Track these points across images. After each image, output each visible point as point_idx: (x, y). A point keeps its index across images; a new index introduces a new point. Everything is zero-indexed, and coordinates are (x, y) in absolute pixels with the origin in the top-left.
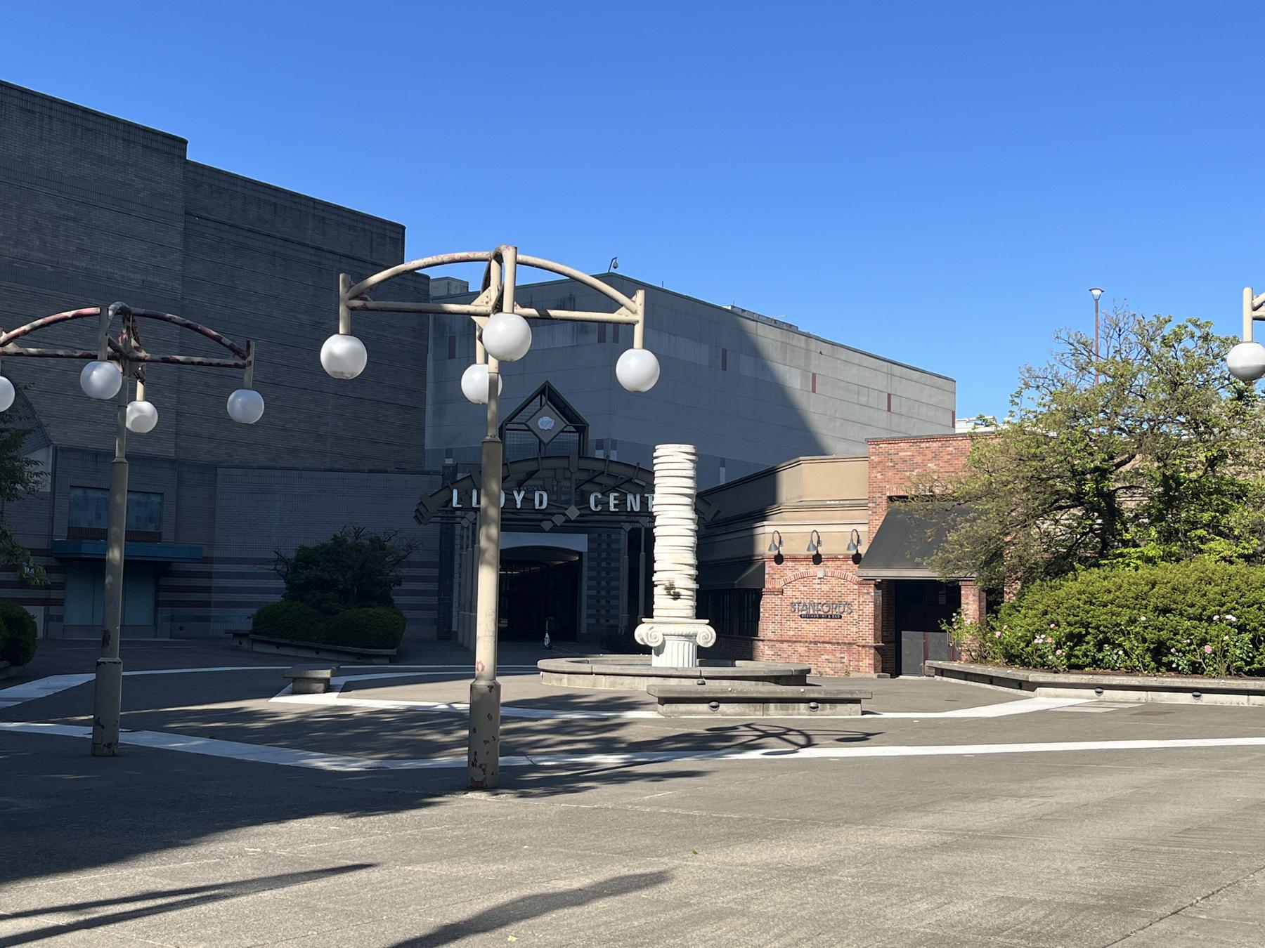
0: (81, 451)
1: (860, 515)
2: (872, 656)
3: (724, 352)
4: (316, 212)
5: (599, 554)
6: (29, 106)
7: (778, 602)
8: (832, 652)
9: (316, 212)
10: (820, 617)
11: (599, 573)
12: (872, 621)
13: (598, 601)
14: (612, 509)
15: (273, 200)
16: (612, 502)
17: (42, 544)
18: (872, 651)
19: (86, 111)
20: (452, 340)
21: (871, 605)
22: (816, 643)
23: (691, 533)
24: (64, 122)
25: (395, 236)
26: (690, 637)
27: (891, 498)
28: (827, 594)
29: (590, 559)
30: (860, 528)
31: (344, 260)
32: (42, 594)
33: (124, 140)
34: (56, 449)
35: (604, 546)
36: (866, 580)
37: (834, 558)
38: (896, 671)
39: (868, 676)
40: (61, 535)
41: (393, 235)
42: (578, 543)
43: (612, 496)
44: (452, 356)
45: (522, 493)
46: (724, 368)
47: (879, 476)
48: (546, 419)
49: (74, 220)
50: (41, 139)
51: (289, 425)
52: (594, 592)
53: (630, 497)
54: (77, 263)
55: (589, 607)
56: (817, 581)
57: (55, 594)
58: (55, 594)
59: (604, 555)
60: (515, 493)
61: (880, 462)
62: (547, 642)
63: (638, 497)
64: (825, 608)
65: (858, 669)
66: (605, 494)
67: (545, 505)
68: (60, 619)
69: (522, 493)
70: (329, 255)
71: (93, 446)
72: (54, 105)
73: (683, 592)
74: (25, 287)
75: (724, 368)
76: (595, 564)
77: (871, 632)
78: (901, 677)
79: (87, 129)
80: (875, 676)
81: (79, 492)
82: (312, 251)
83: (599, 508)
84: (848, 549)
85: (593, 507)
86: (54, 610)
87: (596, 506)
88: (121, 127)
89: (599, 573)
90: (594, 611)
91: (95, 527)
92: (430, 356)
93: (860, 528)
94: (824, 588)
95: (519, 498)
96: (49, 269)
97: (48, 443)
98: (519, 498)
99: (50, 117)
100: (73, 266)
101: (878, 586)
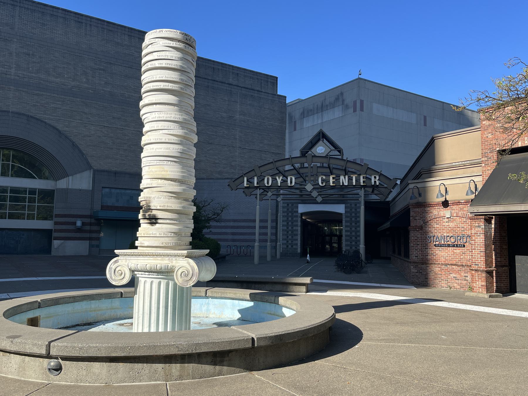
0: (108, 172)
1: (477, 170)
2: (484, 279)
3: (425, 118)
4: (234, 71)
5: (351, 215)
6: (80, 20)
7: (419, 236)
8: (458, 272)
9: (234, 71)
10: (449, 246)
11: (351, 224)
12: (483, 249)
13: (351, 238)
14: (331, 184)
15: (213, 66)
16: (331, 180)
17: (88, 213)
18: (484, 275)
19: (108, 22)
20: (295, 122)
21: (482, 236)
22: (446, 265)
23: (174, 139)
24: (97, 27)
25: (273, 81)
26: (166, 273)
27: (502, 152)
28: (453, 229)
29: (346, 217)
30: (476, 179)
31: (242, 89)
32: (87, 235)
33: (129, 35)
34: (95, 171)
35: (353, 210)
36: (478, 215)
37: (458, 203)
38: (513, 290)
39: (481, 295)
40: (97, 207)
41: (271, 81)
42: (340, 209)
43: (331, 178)
44: (295, 130)
45: (281, 178)
46: (425, 125)
47: (490, 136)
48: (321, 148)
49: (103, 70)
50: (86, 34)
51: (217, 161)
52: (349, 233)
53: (342, 177)
54: (105, 89)
55: (346, 241)
56: (447, 220)
57: (94, 235)
58: (94, 235)
59: (353, 215)
60: (277, 178)
61: (489, 125)
62: (308, 258)
63: (347, 177)
64: (453, 240)
65: (471, 289)
66: (328, 176)
67: (293, 184)
68: (98, 246)
69: (281, 178)
70: (235, 87)
71: (114, 169)
72: (93, 20)
73: (159, 214)
74: (78, 99)
75: (425, 125)
76: (348, 219)
77: (483, 259)
78: (517, 295)
79: (110, 30)
80: (486, 296)
81: (107, 190)
82: (228, 85)
83: (324, 184)
84: (467, 195)
85: (320, 184)
86: (94, 242)
87: (322, 183)
88: (127, 30)
89: (351, 224)
90: (349, 243)
91: (116, 205)
92: (287, 131)
93: (476, 179)
94: (451, 225)
95: (279, 180)
96: (90, 91)
97: (89, 167)
98: (279, 180)
99: (91, 25)
100: (103, 90)
101: (488, 220)
